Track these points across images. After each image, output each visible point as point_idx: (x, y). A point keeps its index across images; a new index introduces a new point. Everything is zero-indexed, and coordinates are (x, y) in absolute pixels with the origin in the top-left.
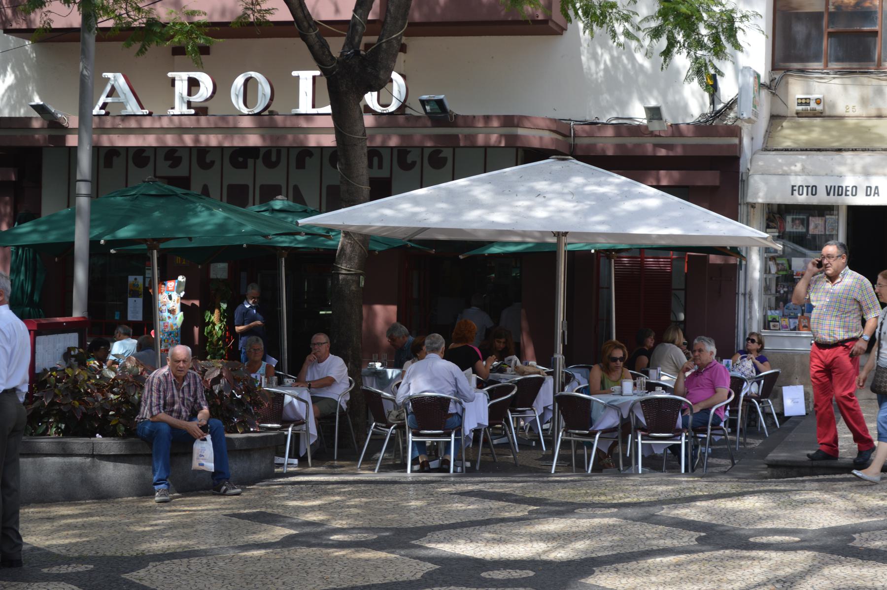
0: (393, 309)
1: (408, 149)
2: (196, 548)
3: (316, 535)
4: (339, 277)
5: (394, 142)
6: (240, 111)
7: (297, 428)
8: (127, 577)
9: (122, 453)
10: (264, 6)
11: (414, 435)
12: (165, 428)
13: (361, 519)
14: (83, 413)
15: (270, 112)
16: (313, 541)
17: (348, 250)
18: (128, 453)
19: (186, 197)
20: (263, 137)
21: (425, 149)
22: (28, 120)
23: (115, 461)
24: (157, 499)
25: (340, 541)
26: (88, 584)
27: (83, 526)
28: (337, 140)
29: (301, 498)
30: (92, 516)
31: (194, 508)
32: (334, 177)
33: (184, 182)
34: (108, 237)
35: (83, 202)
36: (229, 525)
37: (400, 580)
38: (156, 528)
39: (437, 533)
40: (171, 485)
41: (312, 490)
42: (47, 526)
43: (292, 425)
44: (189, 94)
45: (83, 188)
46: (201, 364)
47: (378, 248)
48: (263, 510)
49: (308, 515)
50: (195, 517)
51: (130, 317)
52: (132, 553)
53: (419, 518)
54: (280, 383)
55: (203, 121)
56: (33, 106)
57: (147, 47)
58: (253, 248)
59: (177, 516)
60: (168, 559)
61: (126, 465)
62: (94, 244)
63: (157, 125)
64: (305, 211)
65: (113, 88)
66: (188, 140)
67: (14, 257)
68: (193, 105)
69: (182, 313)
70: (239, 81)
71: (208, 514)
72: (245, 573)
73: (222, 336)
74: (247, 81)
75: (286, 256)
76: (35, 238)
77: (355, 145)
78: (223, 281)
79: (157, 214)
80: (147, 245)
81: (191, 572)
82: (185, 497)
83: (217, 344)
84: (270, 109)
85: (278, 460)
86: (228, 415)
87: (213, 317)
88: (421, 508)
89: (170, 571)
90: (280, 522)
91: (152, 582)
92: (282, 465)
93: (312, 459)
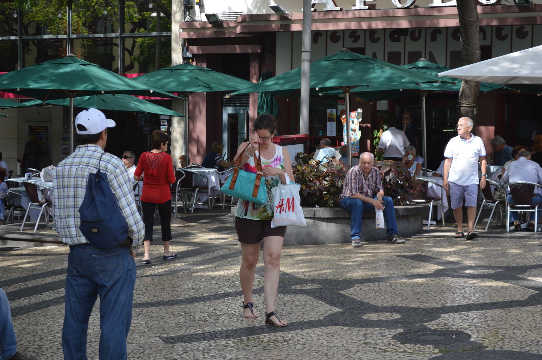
0: (492, 128)
1: (503, 27)
2: (382, 276)
3: (455, 270)
4: (460, 109)
5: (495, 23)
6: (396, 6)
7: (436, 202)
9: (332, 217)
11: (512, 207)
12: (360, 203)
13: (482, 260)
14: (308, 193)
15: (415, 6)
16: (455, 274)
17: (467, 91)
18: (335, 217)
20: (410, 22)
21: (514, 27)
22: (269, 15)
23: (327, 222)
25: (471, 274)
26: (320, 296)
27: (311, 261)
28: (460, 22)
29: (442, 247)
32: (458, 46)
33: (362, 51)
34: (320, 86)
35: (306, 66)
36: (400, 262)
37: (514, 300)
38: (355, 263)
39: (534, 270)
40: (361, 237)
41: (448, 241)
42: (290, 260)
43: (433, 200)
45: (305, 56)
46: (378, 163)
47: (486, 90)
48: (420, 253)
49: (448, 257)
50: (378, 257)
51: (329, 134)
53: (520, 260)
54: (424, 175)
55: (374, 13)
56: (271, 7)
59: (367, 256)
60: (366, 283)
61: (334, 224)
62: (312, 91)
63: (346, 17)
64: (438, 68)
66: (364, 25)
67: (259, 100)
68: (367, 3)
71: (386, 255)
75: (426, 96)
76: (277, 88)
77: (472, 25)
78: (385, 111)
79: (350, 72)
80: (343, 90)
81: (381, 291)
82: (370, 244)
84: (415, 4)
85: (425, 222)
86: (394, 194)
87: (379, 134)
88: (520, 254)
89: (368, 290)
90: (431, 261)
91: (358, 296)
92: (427, 225)
93: (445, 221)
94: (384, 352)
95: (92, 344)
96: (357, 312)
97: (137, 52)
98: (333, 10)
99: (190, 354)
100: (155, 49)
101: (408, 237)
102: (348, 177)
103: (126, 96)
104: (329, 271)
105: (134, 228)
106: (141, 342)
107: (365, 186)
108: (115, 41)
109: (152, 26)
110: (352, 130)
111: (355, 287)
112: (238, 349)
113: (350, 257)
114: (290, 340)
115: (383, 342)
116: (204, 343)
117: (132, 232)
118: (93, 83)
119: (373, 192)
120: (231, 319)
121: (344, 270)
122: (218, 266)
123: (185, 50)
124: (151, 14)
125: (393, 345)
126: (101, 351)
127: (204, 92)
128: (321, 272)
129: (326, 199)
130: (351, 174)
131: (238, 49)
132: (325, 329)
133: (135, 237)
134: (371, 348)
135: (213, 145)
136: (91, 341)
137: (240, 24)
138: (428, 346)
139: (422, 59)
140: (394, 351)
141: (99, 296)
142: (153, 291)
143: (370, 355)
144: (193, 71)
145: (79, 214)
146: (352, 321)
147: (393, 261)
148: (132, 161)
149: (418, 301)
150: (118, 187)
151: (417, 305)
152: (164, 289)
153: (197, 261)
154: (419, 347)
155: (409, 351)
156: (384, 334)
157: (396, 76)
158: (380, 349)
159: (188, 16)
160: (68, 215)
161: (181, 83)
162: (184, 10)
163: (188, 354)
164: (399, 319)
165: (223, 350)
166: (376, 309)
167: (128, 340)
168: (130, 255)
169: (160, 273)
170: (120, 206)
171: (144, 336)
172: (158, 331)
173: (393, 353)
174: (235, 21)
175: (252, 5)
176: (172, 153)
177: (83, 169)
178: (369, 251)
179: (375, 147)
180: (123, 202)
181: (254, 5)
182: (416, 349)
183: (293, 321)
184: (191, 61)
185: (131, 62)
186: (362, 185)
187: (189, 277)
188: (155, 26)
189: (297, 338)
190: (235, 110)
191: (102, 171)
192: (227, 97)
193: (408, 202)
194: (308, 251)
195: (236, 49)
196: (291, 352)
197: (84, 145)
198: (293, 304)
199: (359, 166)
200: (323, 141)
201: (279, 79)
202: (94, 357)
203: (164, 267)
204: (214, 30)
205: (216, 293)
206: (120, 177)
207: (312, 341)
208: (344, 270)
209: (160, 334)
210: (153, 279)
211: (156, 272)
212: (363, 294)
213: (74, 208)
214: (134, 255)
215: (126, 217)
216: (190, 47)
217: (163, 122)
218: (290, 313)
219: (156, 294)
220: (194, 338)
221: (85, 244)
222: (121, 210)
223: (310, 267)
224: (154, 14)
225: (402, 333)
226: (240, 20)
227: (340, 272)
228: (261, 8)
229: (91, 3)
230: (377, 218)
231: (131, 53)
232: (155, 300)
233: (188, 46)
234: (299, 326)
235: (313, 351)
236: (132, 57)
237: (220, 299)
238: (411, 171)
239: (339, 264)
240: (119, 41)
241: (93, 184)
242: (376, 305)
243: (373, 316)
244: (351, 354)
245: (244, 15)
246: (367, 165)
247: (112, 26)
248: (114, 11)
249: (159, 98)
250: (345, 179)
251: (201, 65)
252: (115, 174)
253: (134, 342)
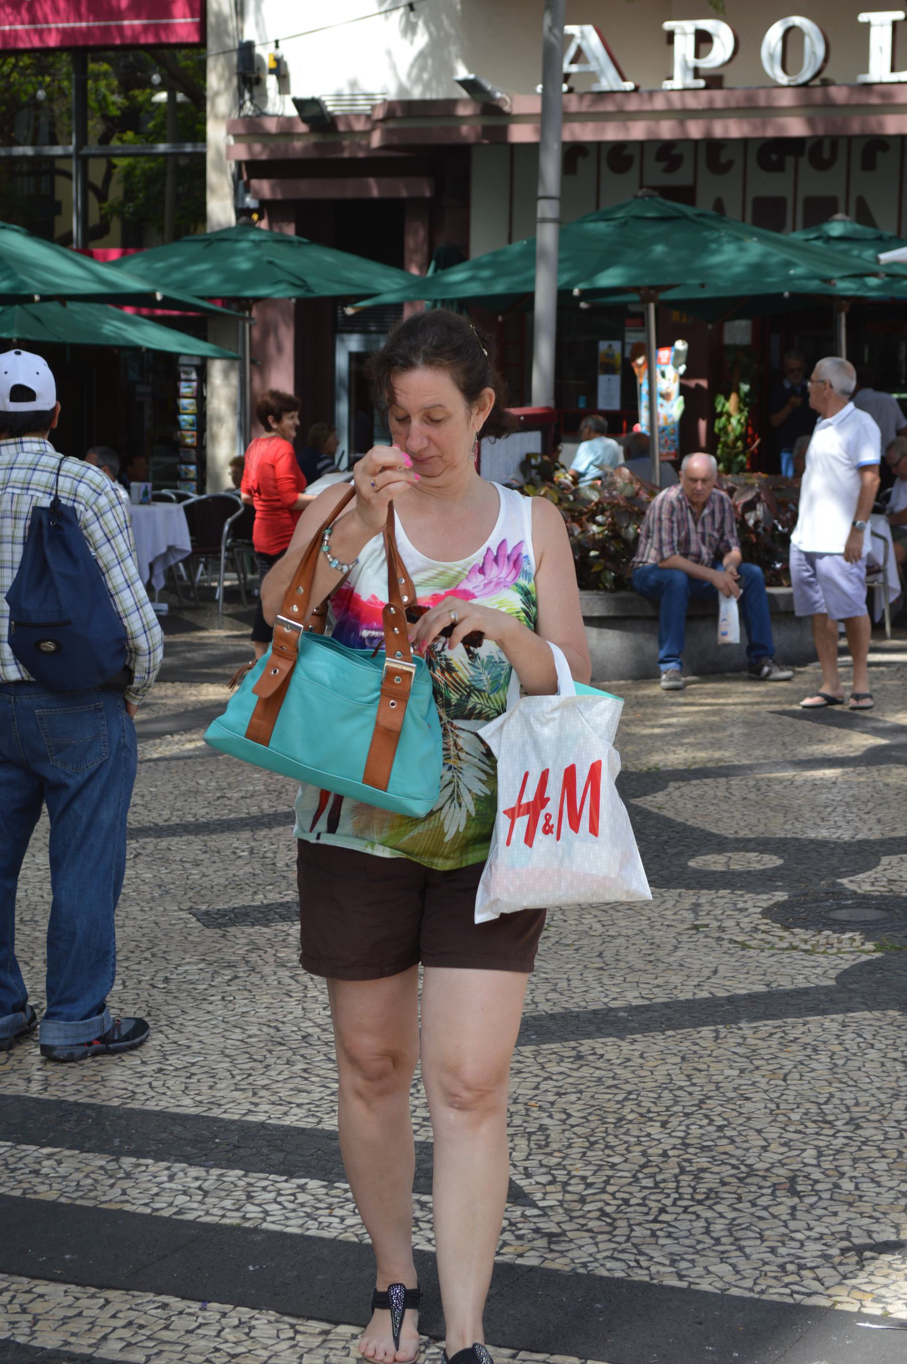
2: (736, 763)
6: (774, 81)
8: (639, 804)
12: (681, 579)
18: (619, 614)
20: (811, 122)
22: (451, 103)
23: (600, 626)
31: (722, 701)
33: (686, 195)
34: (584, 286)
36: (779, 727)
38: (669, 730)
41: (899, 675)
44: (697, 55)
45: (547, 209)
51: (602, 405)
52: (640, 767)
55: (719, 97)
59: (697, 712)
60: (697, 778)
62: (563, 297)
63: (647, 107)
64: (880, 238)
65: (579, 51)
66: (695, 130)
68: (701, 73)
70: (774, 35)
71: (745, 711)
74: (788, 32)
76: (474, 289)
83: (734, 446)
84: (824, 75)
89: (701, 797)
91: (677, 813)
93: (893, 625)
94: (743, 949)
95: (26, 928)
96: (674, 851)
97: (116, 191)
101: (800, 665)
102: (651, 514)
103: (94, 309)
105: (142, 642)
106: (144, 924)
107: (694, 537)
108: (60, 165)
109: (155, 126)
115: (738, 924)
117: (136, 651)
118: (11, 276)
119: (715, 554)
124: (152, 95)
125: (763, 932)
127: (290, 298)
129: (596, 569)
130: (661, 508)
131: (374, 189)
133: (141, 665)
134: (710, 940)
136: (21, 920)
137: (380, 125)
138: (849, 935)
139: (839, 216)
141: (45, 808)
143: (709, 955)
147: (763, 724)
151: (823, 833)
154: (828, 937)
156: (740, 905)
157: (774, 260)
158: (731, 941)
159: (248, 104)
161: (232, 276)
163: (261, 952)
164: (777, 869)
166: (721, 844)
168: (124, 711)
170: (110, 586)
171: (151, 909)
172: (186, 897)
173: (762, 951)
174: (368, 117)
175: (409, 75)
176: (209, 451)
180: (116, 578)
182: (821, 942)
184: (255, 217)
185: (102, 217)
186: (688, 535)
188: (162, 125)
190: (367, 343)
191: (64, 501)
192: (350, 311)
195: (368, 188)
197: (12, 440)
199: (680, 487)
200: (588, 423)
201: (479, 266)
202: (32, 959)
203: (194, 737)
206: (109, 516)
209: (190, 904)
212: (690, 805)
214: (133, 708)
215: (122, 615)
216: (254, 182)
217: (186, 373)
219: (179, 805)
220: (276, 913)
222: (112, 596)
224: (162, 96)
225: (785, 901)
226: (379, 114)
227: (631, 753)
231: (102, 196)
232: (175, 820)
233: (250, 177)
235: (569, 945)
236: (106, 205)
240: (73, 168)
241: (45, 533)
243: (715, 862)
244: (660, 953)
246: (699, 486)
247: (52, 124)
249: (175, 313)
250: (646, 519)
251: (280, 229)
252: (96, 510)
253: (127, 923)
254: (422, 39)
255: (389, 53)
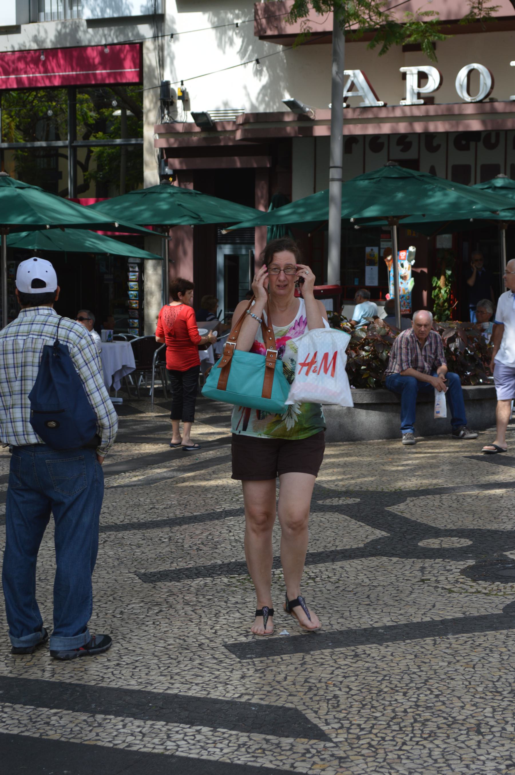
2: (445, 486)
6: (463, 100)
10: (486, 5)
12: (413, 381)
18: (378, 402)
19: (422, 178)
20: (484, 122)
24: (404, 441)
26: (358, 515)
27: (345, 465)
30: (351, 456)
31: (437, 451)
34: (356, 216)
35: (335, 188)
36: (470, 466)
38: (407, 468)
44: (419, 86)
45: (335, 173)
46: (438, 326)
50: (439, 458)
51: (368, 283)
52: (391, 489)
55: (432, 109)
57: (388, 47)
58: (479, 221)
59: (423, 457)
60: (423, 495)
61: (377, 412)
62: (345, 223)
63: (391, 115)
66: (418, 128)
67: (269, 235)
68: (422, 96)
69: (413, 279)
70: (463, 74)
71: (450, 456)
72: (491, 509)
73: (447, 298)
74: (470, 72)
76: (294, 219)
79: (400, 195)
80: (388, 221)
81: (444, 506)
82: (427, 440)
83: (443, 306)
84: (491, 96)
87: (439, 282)
89: (426, 506)
91: (412, 515)
94: (449, 593)
96: (410, 537)
97: (93, 166)
98: (373, 105)
99: (178, 596)
100: (120, 162)
101: (481, 430)
102: (396, 345)
103: (81, 233)
104: (370, 479)
105: (106, 421)
107: (420, 358)
109: (114, 129)
110: (402, 277)
111: (408, 501)
112: (245, 589)
113: (400, 459)
114: (317, 577)
115: (447, 579)
116: (197, 582)
117: (102, 426)
118: (33, 214)
120: (234, 547)
121: (393, 478)
122: (213, 472)
123: (163, 164)
124: (113, 112)
125: (461, 583)
126: (56, 592)
127: (190, 225)
128: (359, 481)
129: (365, 376)
130: (401, 341)
132: (366, 561)
133: (106, 434)
134: (430, 588)
135: (203, 299)
136: (40, 579)
137: (241, 127)
139: (501, 175)
140: (464, 591)
142: (124, 508)
144: (175, 195)
145: (29, 402)
146: (403, 549)
147: (461, 464)
148: (90, 324)
149: (497, 520)
150: (84, 364)
151: (494, 526)
152: (139, 505)
153: (184, 466)
154: (498, 586)
155: (484, 591)
156: (448, 568)
157: (464, 200)
158: (443, 588)
159: (167, 116)
160: (13, 405)
161: (158, 213)
162: (161, 107)
163: (175, 597)
164: (468, 546)
165: (224, 591)
166: (437, 533)
167: (94, 578)
169: (133, 484)
171: (113, 572)
172: (133, 565)
173: (461, 594)
174: (234, 122)
175: (257, 99)
177: (34, 340)
178: (426, 451)
179: (434, 301)
180: (90, 386)
181: (260, 99)
183: (321, 550)
184: (171, 179)
185: (85, 180)
186: (417, 356)
187: (173, 488)
188: (119, 129)
189: (327, 573)
190: (234, 250)
191: (61, 342)
192: (224, 232)
193: (481, 380)
194: (340, 450)
196: (319, 593)
197: (32, 308)
198: (320, 526)
201: (297, 206)
203: (137, 474)
204: (203, 135)
205: (212, 511)
206: (87, 350)
207: (348, 578)
208: (392, 477)
209: (135, 569)
210: (123, 492)
211: (126, 481)
212: (419, 511)
213: (21, 394)
215: (94, 406)
216: (170, 160)
217: (132, 267)
218: (317, 538)
219: (129, 512)
220: (184, 574)
221: (35, 445)
222: (88, 395)
223: (344, 473)
224: (118, 112)
226: (240, 121)
228: (271, 104)
229: (28, 97)
230: (436, 403)
231: (85, 168)
232: (127, 521)
233: (167, 158)
234: (329, 556)
236: (87, 173)
237: (217, 519)
238: (486, 336)
239: (384, 468)
240: (68, 152)
241: (51, 360)
242: (438, 526)
243: (433, 543)
244: (402, 595)
245: (247, 115)
246: (423, 328)
247: (57, 129)
248: (61, 108)
251: (185, 186)
252: (79, 347)
253: (100, 580)
254: (265, 79)
255: (245, 88)
